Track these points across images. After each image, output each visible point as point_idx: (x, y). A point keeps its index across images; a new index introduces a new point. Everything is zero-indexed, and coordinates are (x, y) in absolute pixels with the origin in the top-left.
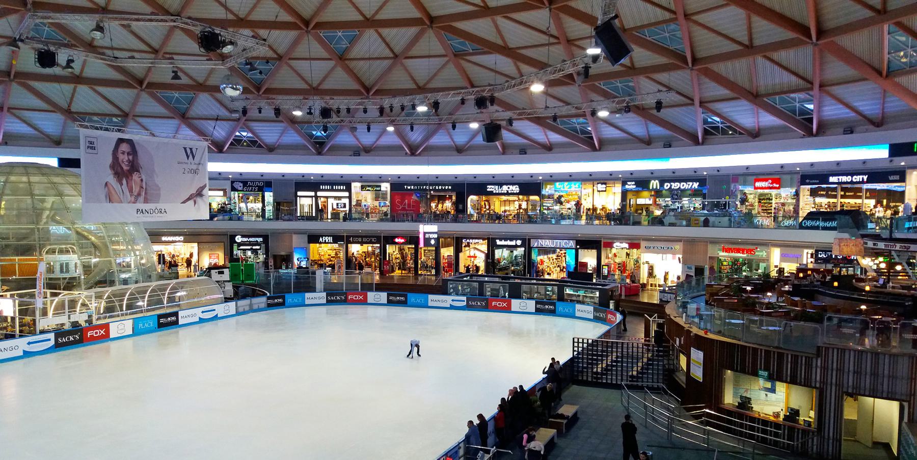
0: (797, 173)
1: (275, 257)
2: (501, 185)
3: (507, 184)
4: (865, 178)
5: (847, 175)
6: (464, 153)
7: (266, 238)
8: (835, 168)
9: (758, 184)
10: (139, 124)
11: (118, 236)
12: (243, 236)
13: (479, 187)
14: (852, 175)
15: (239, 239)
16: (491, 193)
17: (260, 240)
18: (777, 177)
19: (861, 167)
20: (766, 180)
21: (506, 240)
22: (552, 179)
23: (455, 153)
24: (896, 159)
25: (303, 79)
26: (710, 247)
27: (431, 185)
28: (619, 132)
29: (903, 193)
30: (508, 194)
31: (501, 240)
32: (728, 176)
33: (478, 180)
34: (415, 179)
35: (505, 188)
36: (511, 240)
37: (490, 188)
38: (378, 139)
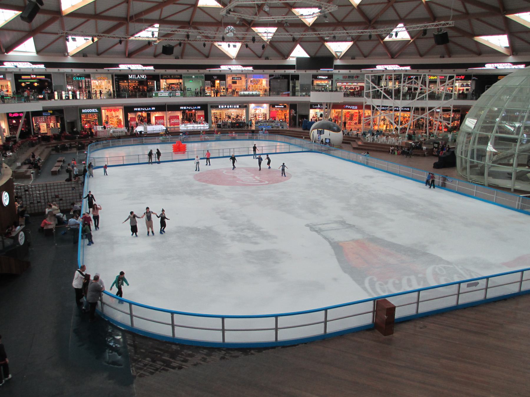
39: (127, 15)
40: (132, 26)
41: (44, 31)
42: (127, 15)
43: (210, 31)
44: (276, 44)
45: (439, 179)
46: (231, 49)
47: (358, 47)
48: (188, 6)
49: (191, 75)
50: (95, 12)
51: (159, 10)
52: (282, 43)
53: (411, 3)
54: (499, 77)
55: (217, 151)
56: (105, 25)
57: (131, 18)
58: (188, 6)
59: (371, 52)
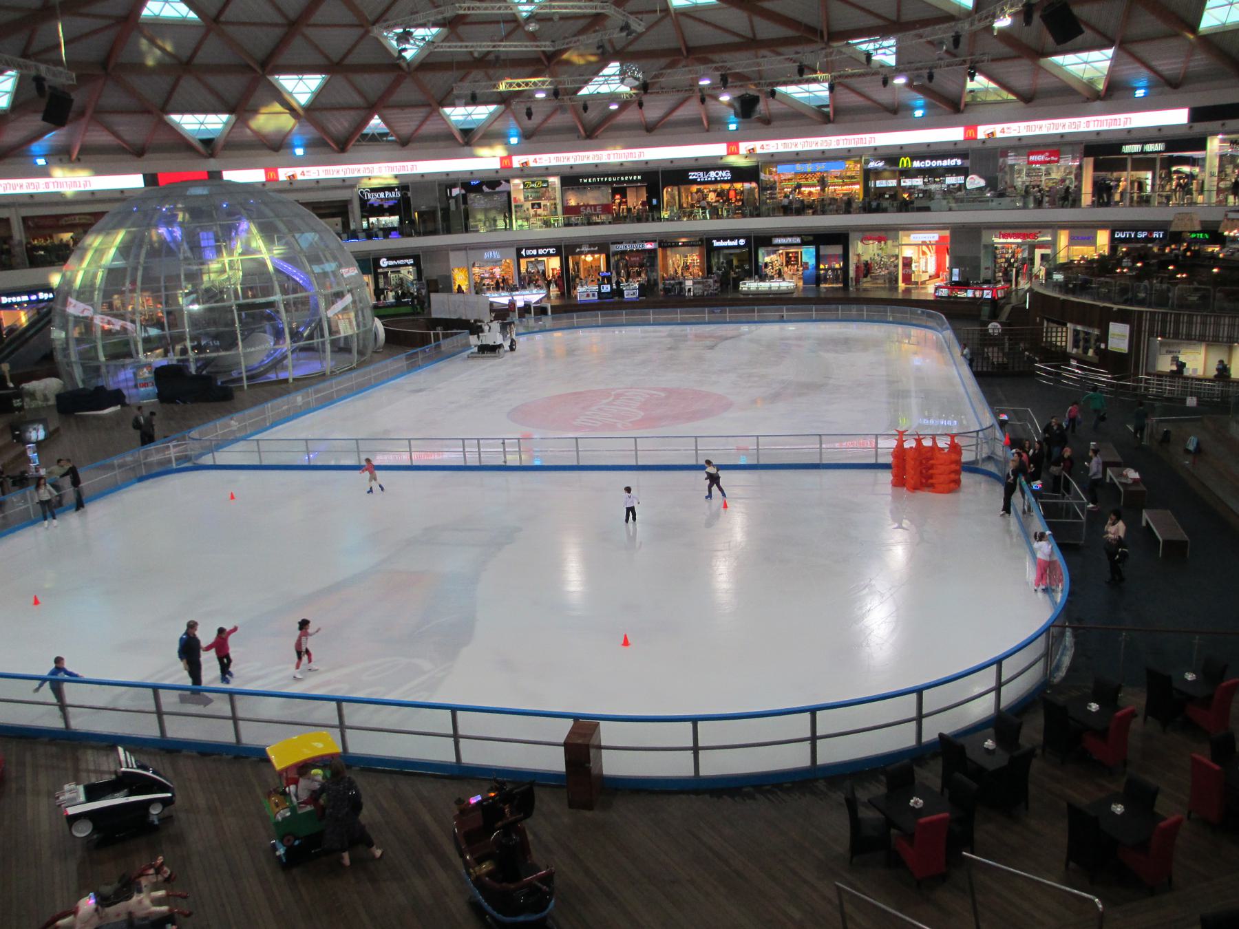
1: (429, 282)
2: (706, 170)
3: (714, 169)
6: (655, 132)
7: (417, 259)
8: (694, 163)
9: (1032, 158)
10: (878, 16)
11: (389, 266)
12: (389, 259)
13: (677, 175)
15: (384, 263)
16: (694, 182)
17: (411, 261)
18: (1055, 148)
19: (1156, 134)
21: (725, 240)
22: (775, 160)
23: (644, 133)
25: (321, 52)
27: (613, 175)
28: (861, 99)
29: (1204, 159)
30: (716, 182)
31: (718, 240)
32: (996, 148)
33: (675, 166)
34: (924, 149)
35: (712, 174)
36: (732, 239)
37: (693, 176)
38: (420, 126)
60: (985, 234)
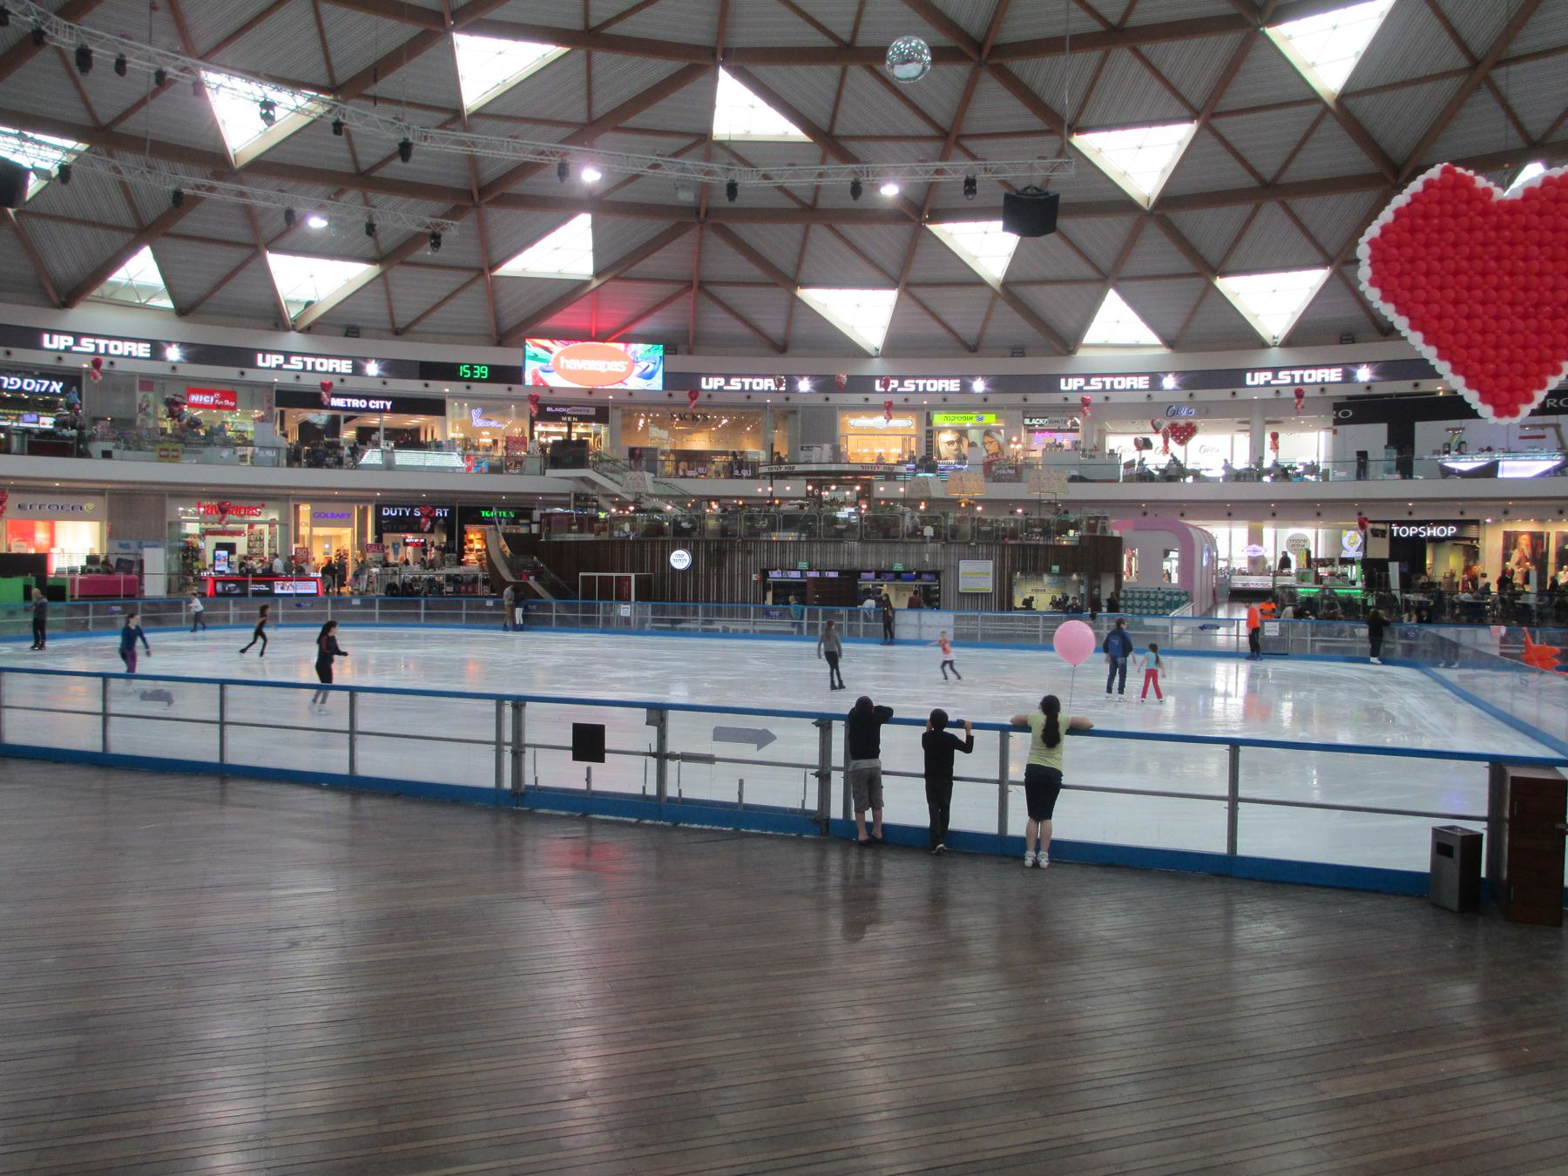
0: (270, 385)
4: (389, 405)
5: (359, 397)
14: (368, 398)
18: (227, 388)
20: (210, 393)
24: (675, 393)
26: (169, 503)
39: (925, 201)
40: (499, 218)
41: (411, 258)
42: (925, 201)
43: (776, 240)
44: (1020, 291)
45: (1311, 691)
46: (861, 313)
47: (386, 284)
48: (688, 141)
49: (995, 399)
50: (355, 161)
51: (1249, 208)
52: (1049, 288)
53: (626, 33)
54: (13, 500)
55: (480, 720)
56: (401, 217)
57: (484, 190)
58: (688, 141)
59: (418, 320)
60: (169, 503)
